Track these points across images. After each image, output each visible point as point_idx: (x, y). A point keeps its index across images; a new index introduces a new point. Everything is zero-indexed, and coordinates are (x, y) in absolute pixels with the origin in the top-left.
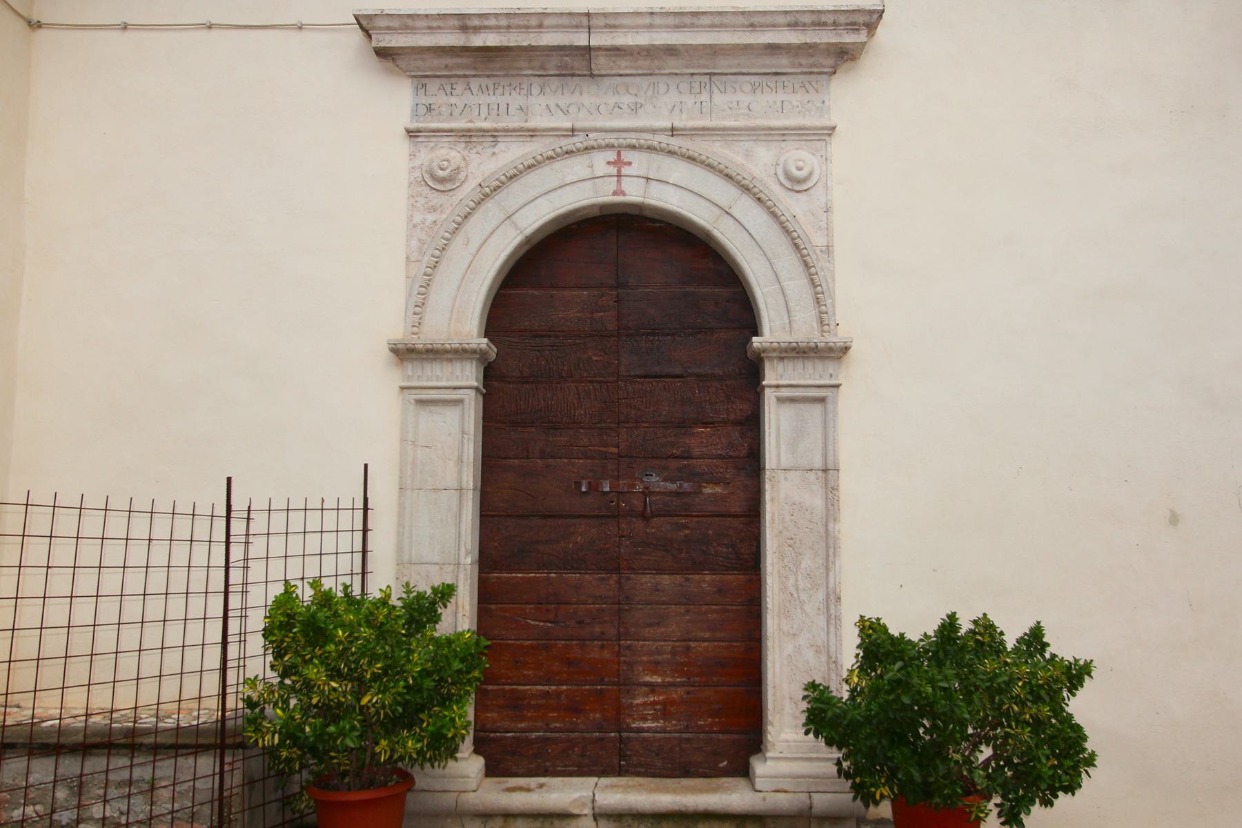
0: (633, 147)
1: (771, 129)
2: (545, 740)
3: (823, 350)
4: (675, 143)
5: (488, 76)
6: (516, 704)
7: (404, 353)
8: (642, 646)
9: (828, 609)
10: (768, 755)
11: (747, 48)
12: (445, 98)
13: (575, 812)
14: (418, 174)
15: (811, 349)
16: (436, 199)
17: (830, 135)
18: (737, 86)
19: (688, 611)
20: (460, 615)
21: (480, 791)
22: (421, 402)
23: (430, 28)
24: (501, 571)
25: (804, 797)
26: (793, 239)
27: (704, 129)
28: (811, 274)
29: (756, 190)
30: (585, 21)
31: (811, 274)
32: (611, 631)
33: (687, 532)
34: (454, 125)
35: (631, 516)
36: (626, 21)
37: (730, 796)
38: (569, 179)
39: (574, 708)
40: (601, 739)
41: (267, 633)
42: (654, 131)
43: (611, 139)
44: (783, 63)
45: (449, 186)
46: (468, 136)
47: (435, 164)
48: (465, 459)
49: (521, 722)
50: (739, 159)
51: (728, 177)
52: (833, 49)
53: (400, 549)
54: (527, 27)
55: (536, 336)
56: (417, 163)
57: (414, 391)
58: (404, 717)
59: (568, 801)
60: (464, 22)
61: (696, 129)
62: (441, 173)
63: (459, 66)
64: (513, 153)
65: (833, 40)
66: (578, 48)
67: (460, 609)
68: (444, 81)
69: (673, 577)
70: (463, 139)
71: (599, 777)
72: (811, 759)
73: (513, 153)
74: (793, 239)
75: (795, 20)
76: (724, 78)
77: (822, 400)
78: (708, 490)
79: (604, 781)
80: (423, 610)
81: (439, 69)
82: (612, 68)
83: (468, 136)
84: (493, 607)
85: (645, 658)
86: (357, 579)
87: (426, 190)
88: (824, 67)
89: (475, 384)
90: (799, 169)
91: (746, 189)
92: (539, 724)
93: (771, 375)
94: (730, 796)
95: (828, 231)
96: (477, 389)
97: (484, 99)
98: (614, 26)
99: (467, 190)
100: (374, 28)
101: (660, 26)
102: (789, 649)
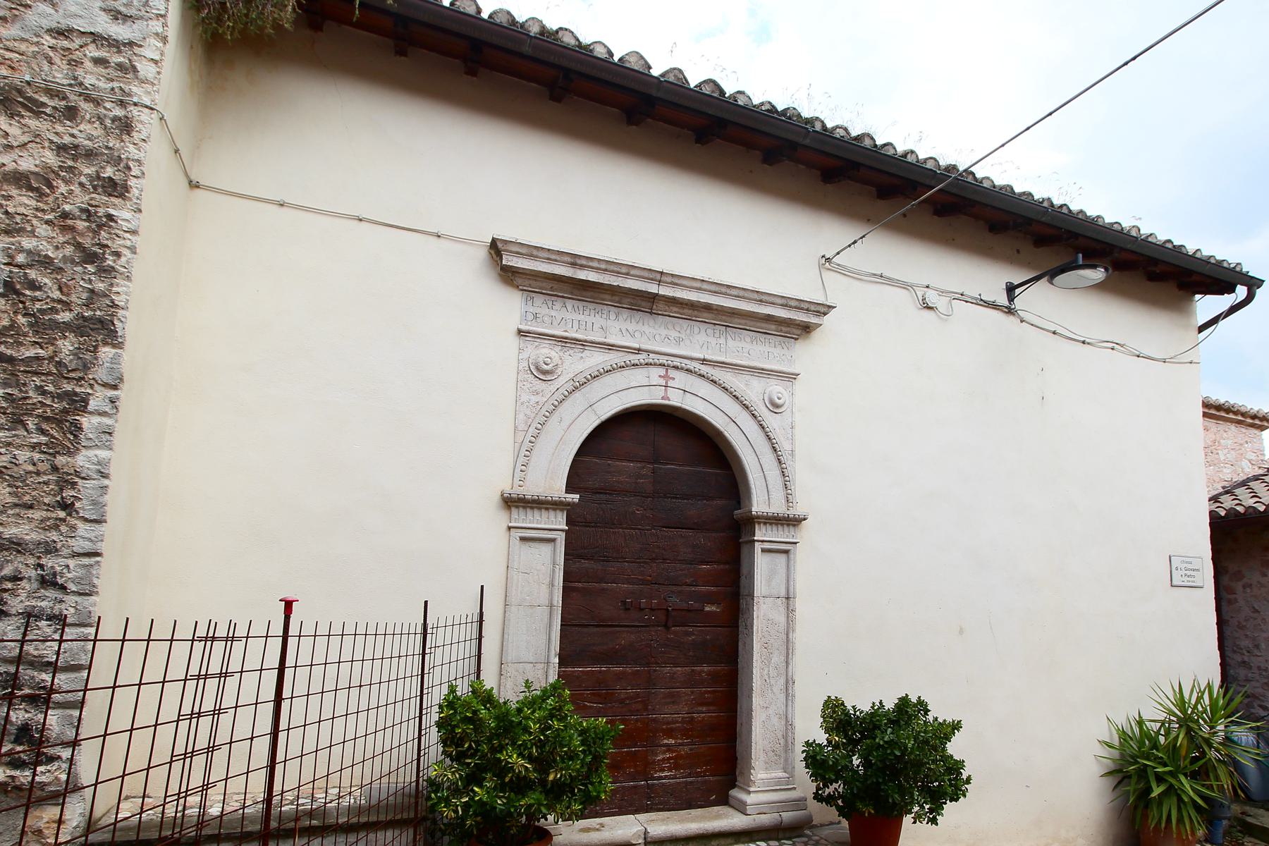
0: (676, 368)
4: (704, 369)
7: (511, 502)
16: (540, 385)
22: (523, 539)
40: (635, 787)
41: (440, 724)
43: (663, 360)
46: (563, 341)
50: (742, 386)
56: (525, 355)
60: (575, 260)
62: (545, 367)
64: (596, 359)
75: (786, 303)
83: (563, 341)
93: (761, 533)
97: (576, 317)
99: (562, 381)
102: (763, 717)
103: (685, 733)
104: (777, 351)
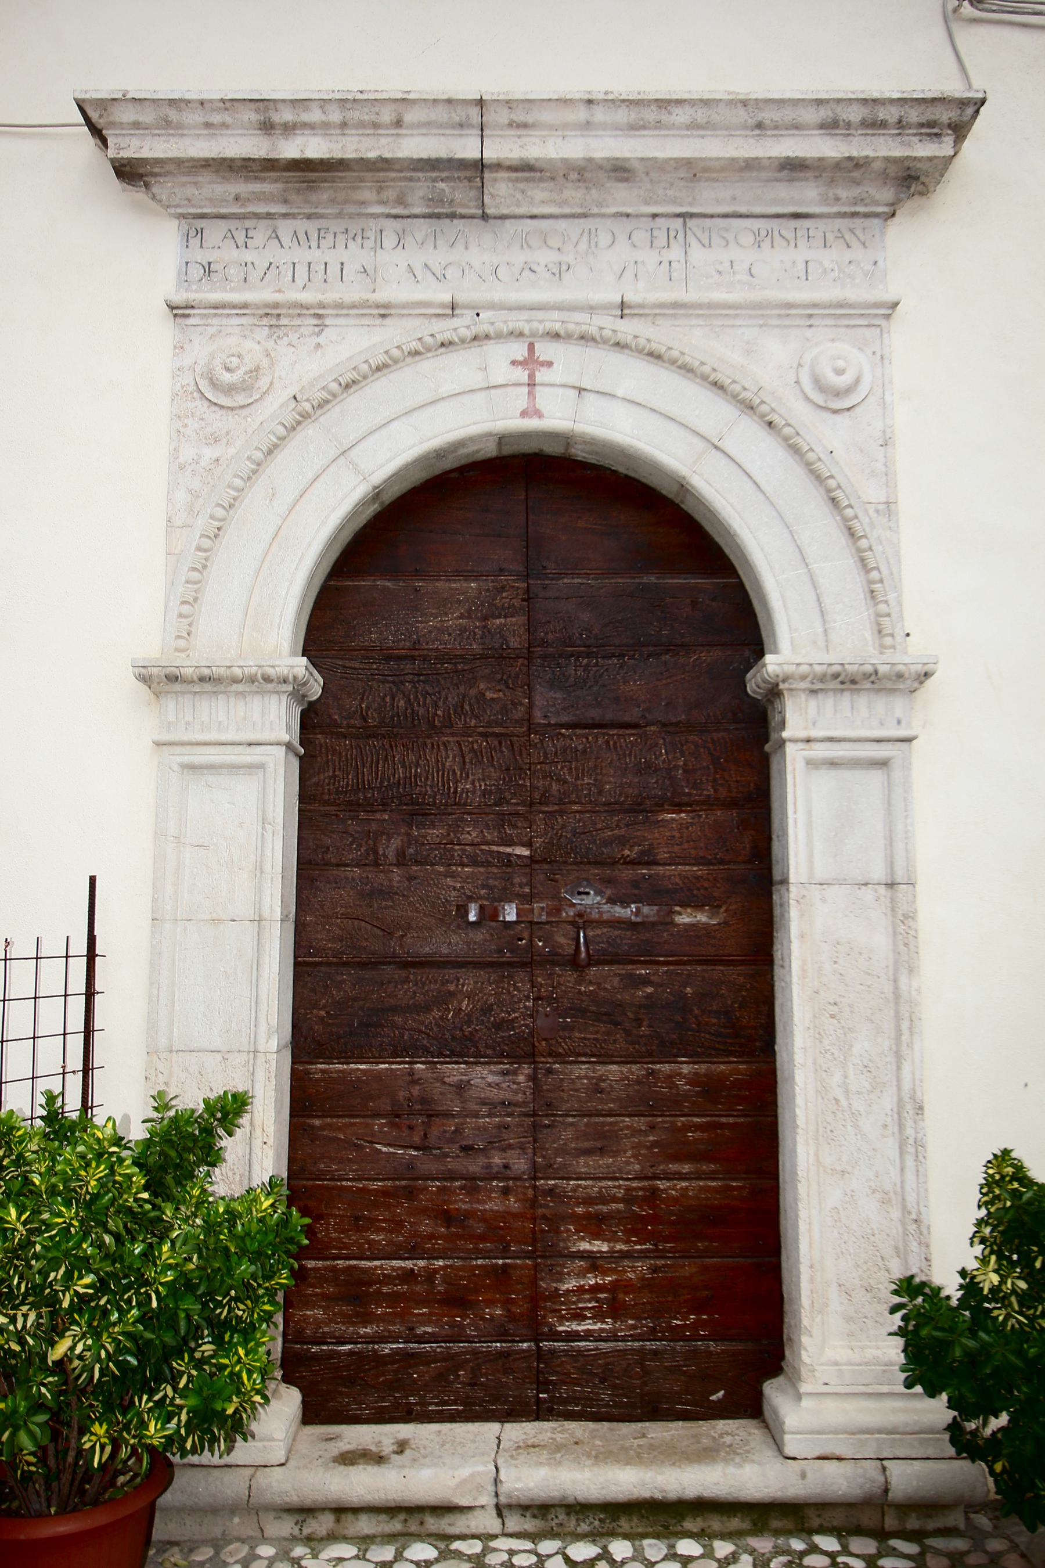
1: (789, 306)
2: (407, 1358)
3: (888, 677)
4: (627, 329)
5: (309, 217)
6: (357, 1293)
7: (163, 682)
8: (575, 1189)
9: (901, 1126)
10: (804, 1388)
11: (750, 165)
12: (235, 253)
13: (464, 1502)
14: (188, 379)
15: (867, 676)
16: (219, 421)
17: (888, 317)
18: (730, 236)
19: (652, 1127)
20: (257, 1143)
21: (292, 1463)
23: (208, 125)
24: (329, 1059)
25: (871, 1469)
26: (829, 491)
27: (675, 305)
28: (859, 550)
29: (764, 408)
30: (474, 112)
31: (859, 550)
32: (520, 1165)
33: (650, 990)
34: (249, 296)
35: (554, 964)
36: (547, 116)
37: (737, 1468)
38: (445, 390)
39: (457, 1300)
42: (591, 309)
43: (519, 321)
44: (807, 195)
45: (240, 399)
46: (272, 315)
47: (217, 362)
48: (267, 867)
49: (365, 1323)
51: (717, 386)
52: (896, 160)
53: (152, 1026)
54: (376, 126)
55: (388, 658)
56: (187, 361)
57: (179, 750)
58: (147, 1366)
59: (452, 1483)
60: (265, 112)
61: (661, 306)
62: (227, 377)
63: (259, 197)
64: (351, 343)
65: (898, 152)
66: (463, 164)
67: (258, 1132)
68: (233, 224)
69: (625, 1069)
70: (265, 321)
71: (502, 1422)
72: (880, 1395)
73: (351, 343)
74: (829, 491)
76: (708, 222)
77: (883, 764)
78: (684, 918)
79: (516, 1432)
80: (185, 1144)
81: (223, 201)
82: (518, 204)
83: (272, 315)
84: (317, 1122)
85: (579, 1210)
86: (75, 1083)
87: (202, 406)
88: (876, 203)
89: (286, 738)
90: (840, 372)
91: (749, 407)
92: (396, 1328)
94: (737, 1468)
95: (888, 476)
96: (289, 746)
97: (302, 255)
98: (525, 126)
99: (273, 408)
100: (112, 124)
101: (604, 126)
103: (636, 1227)
104: (830, 257)
